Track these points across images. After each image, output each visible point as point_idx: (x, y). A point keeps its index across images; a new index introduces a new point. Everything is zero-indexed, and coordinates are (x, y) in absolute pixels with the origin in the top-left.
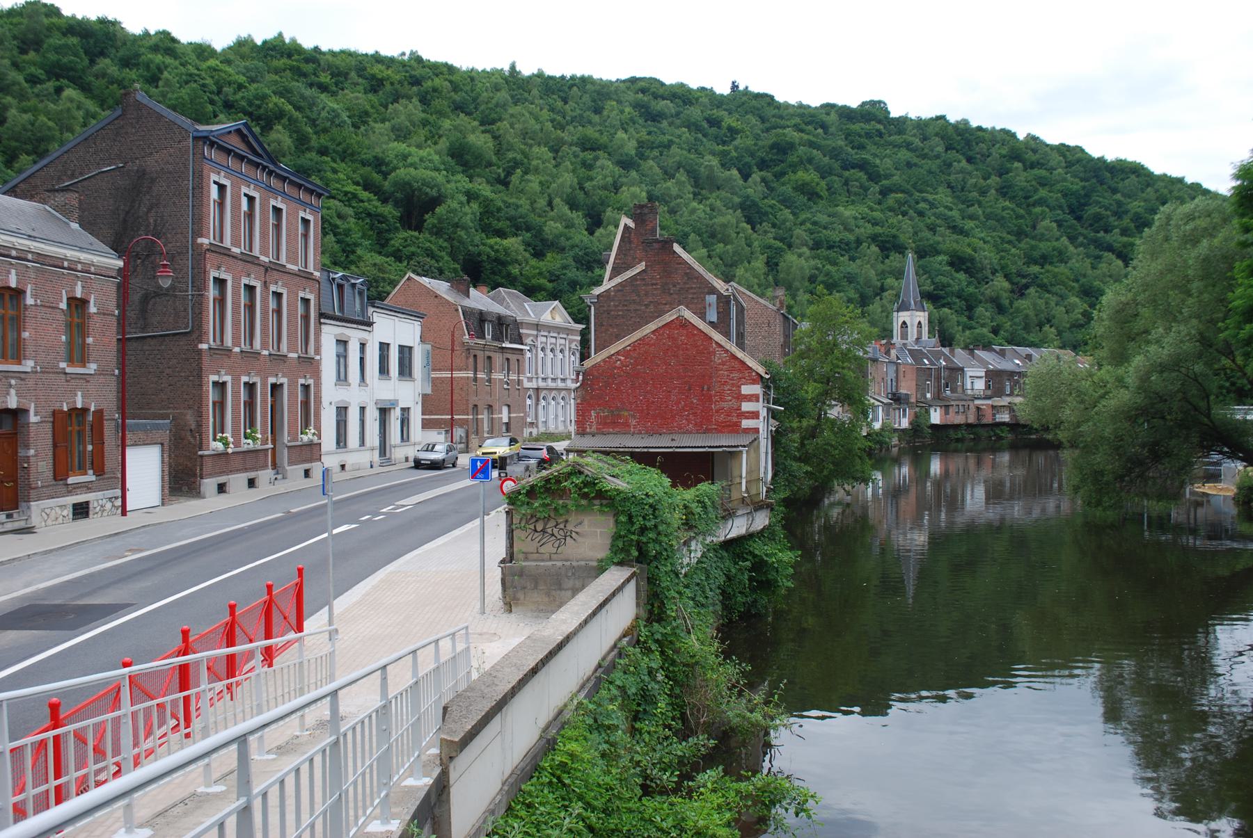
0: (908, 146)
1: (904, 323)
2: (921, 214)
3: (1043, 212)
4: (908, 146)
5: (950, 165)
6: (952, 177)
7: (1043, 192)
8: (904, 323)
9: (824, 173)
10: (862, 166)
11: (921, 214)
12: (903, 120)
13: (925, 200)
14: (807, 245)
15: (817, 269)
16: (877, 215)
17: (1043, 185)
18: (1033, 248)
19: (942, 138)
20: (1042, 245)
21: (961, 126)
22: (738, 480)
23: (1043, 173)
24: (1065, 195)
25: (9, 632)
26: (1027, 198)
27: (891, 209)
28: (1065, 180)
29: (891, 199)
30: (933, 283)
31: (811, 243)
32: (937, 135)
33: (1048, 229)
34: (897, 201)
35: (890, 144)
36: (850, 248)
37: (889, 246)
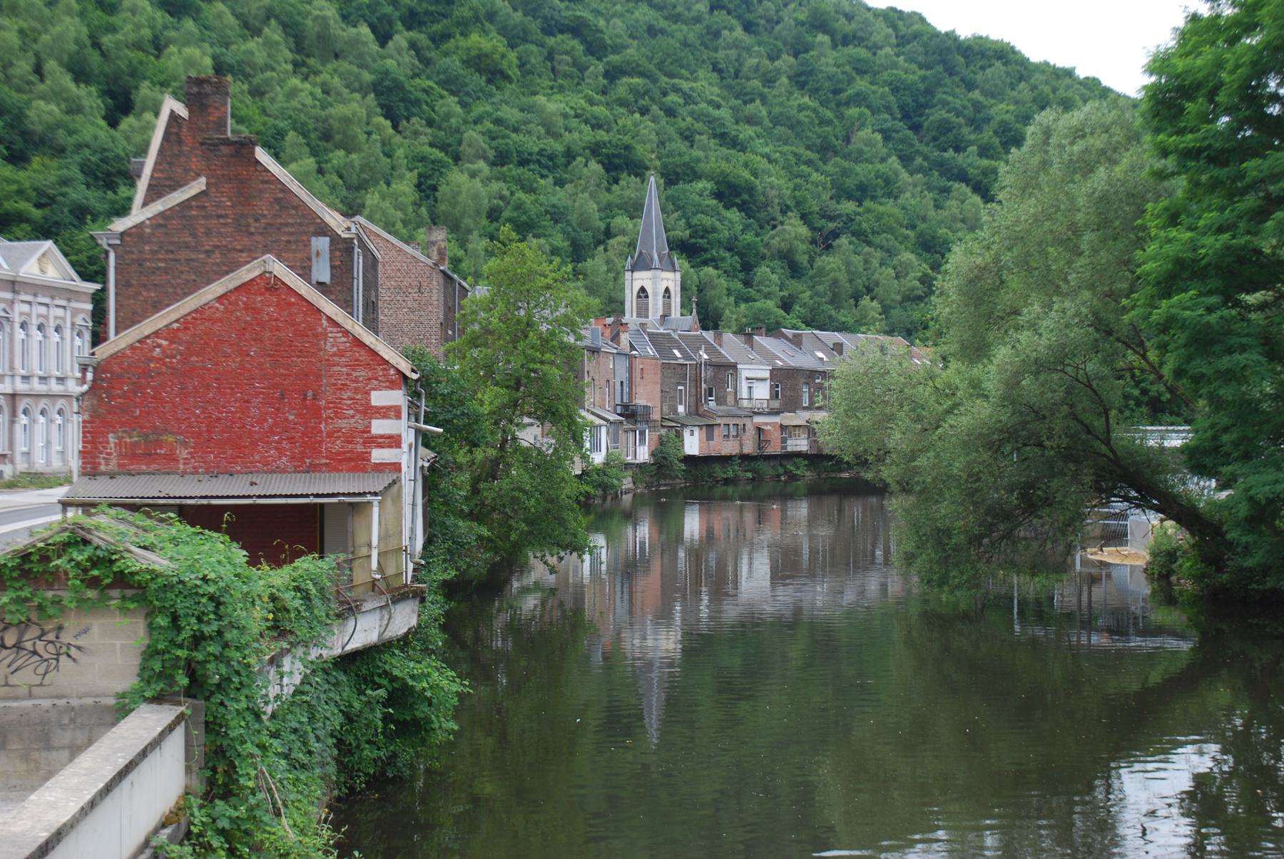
1: (643, 290)
2: (670, 112)
3: (861, 115)
5: (717, 35)
6: (721, 55)
7: (861, 84)
8: (643, 290)
9: (515, 38)
11: (670, 112)
13: (677, 90)
14: (485, 159)
15: (502, 197)
16: (600, 111)
18: (845, 173)
23: (862, 53)
24: (895, 90)
26: (836, 92)
27: (622, 103)
28: (895, 65)
29: (625, 84)
30: (689, 225)
31: (491, 154)
33: (868, 143)
34: (633, 90)
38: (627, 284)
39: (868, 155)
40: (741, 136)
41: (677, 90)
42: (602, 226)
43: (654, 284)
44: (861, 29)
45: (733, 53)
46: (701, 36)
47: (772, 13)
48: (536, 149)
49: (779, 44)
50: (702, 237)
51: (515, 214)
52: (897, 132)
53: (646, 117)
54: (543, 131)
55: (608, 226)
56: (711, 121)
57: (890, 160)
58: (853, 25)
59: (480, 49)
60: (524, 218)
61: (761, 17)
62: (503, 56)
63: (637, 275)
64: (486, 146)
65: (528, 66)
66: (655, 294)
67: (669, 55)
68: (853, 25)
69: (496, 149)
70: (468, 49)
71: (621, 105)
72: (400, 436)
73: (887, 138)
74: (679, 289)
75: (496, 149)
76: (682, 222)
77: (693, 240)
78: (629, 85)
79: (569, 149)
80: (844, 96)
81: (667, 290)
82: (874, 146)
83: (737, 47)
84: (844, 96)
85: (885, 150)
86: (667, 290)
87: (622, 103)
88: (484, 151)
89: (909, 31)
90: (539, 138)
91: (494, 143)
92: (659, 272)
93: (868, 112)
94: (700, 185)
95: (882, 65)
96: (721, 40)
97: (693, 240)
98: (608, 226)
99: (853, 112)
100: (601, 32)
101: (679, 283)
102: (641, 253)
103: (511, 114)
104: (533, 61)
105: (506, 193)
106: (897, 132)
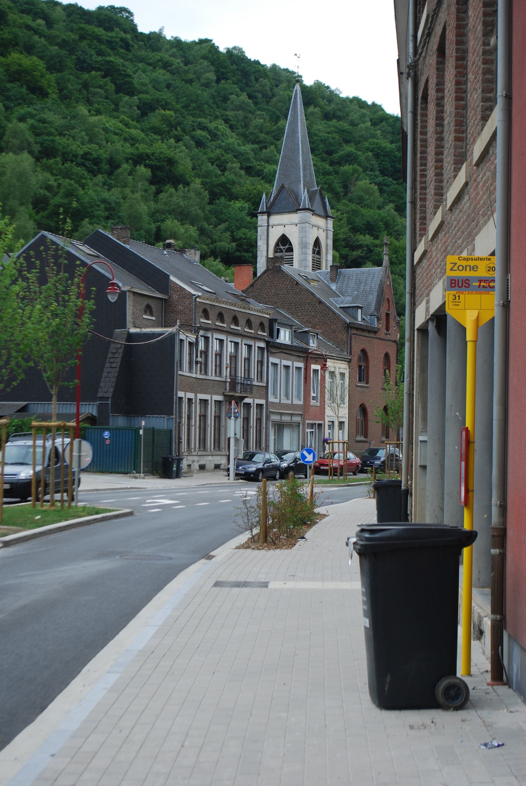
0: (166, 66)
1: (284, 240)
2: (199, 144)
3: (355, 171)
4: (166, 66)
5: (225, 99)
6: (230, 114)
7: (349, 148)
8: (284, 240)
9: (54, 66)
10: (109, 71)
11: (199, 144)
12: (154, 40)
13: (204, 128)
14: (31, 152)
15: (48, 188)
16: (135, 132)
17: (347, 142)
18: (355, 213)
19: (212, 64)
20: (364, 211)
21: (236, 52)
22: (183, 501)
23: (344, 125)
24: (377, 156)
25: (490, 609)
26: (330, 153)
27: (156, 131)
28: (374, 136)
29: (154, 119)
30: (234, 240)
31: (36, 148)
32: (205, 57)
33: (367, 191)
34: (165, 120)
35: (142, 60)
36: (106, 168)
37: (164, 175)
38: (261, 231)
39: (368, 202)
40: (265, 170)
41: (204, 128)
42: (153, 227)
43: (303, 231)
44: (340, 110)
45: (241, 114)
46: (213, 97)
47: (268, 88)
48: (81, 152)
49: (278, 113)
50: (247, 251)
51: (66, 201)
52: (388, 186)
53: (180, 143)
54: (86, 138)
55: (159, 229)
56: (238, 156)
57: (387, 208)
58: (333, 106)
59: (20, 65)
60: (75, 204)
61: (258, 92)
62: (42, 76)
63: (275, 219)
64: (32, 139)
65: (65, 91)
66: (303, 246)
67: (192, 101)
68: (333, 106)
69: (42, 144)
70: (8, 65)
71: (155, 133)
72: (178, 475)
73: (381, 191)
74: (330, 242)
75: (42, 144)
76: (228, 234)
77: (238, 254)
78: (163, 116)
79: (111, 158)
80: (336, 156)
81: (317, 243)
82: (372, 194)
83: (244, 109)
84: (336, 156)
85: (381, 199)
86: (317, 243)
87: (156, 131)
88: (29, 144)
89: (376, 116)
90: (83, 144)
91: (39, 139)
92: (308, 214)
93: (360, 169)
94: (238, 204)
95: (362, 136)
96: (229, 103)
97: (238, 254)
98: (159, 229)
99: (347, 168)
100: (130, 76)
101: (331, 234)
102: (282, 188)
103: (55, 119)
104: (70, 86)
105: (52, 183)
106: (388, 186)
